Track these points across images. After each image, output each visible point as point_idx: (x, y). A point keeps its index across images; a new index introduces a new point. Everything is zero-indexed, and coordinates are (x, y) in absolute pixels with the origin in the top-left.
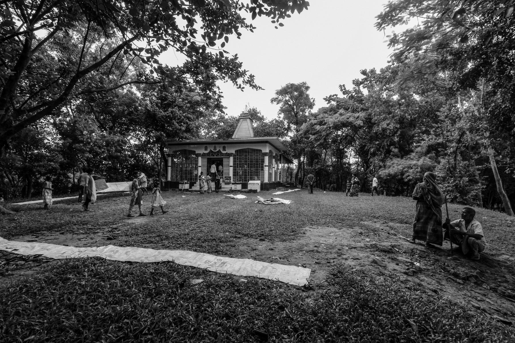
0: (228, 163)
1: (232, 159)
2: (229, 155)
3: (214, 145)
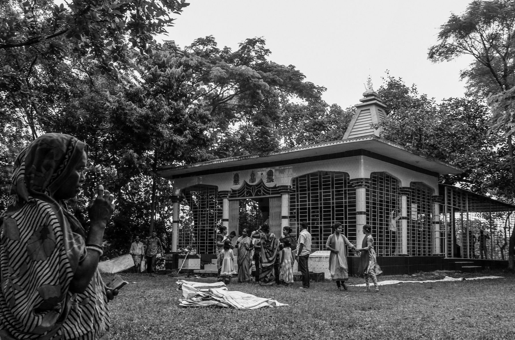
0: (277, 210)
1: (286, 198)
2: (284, 189)
3: (250, 171)
